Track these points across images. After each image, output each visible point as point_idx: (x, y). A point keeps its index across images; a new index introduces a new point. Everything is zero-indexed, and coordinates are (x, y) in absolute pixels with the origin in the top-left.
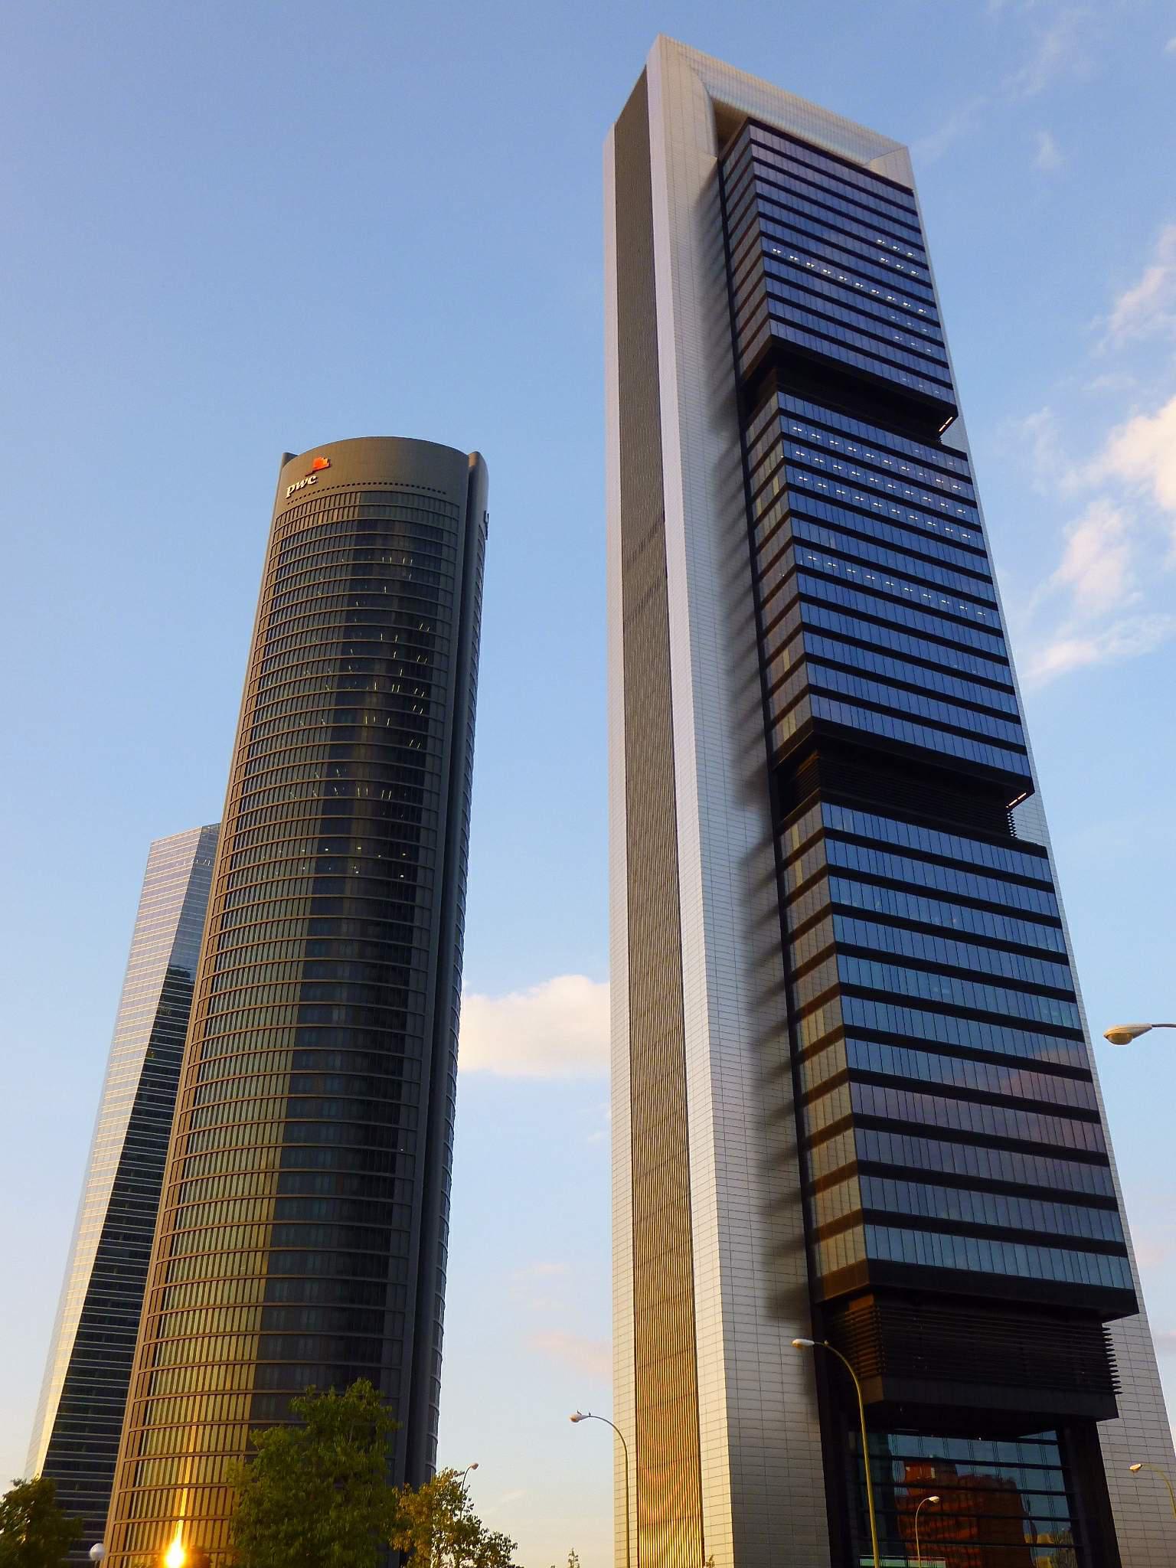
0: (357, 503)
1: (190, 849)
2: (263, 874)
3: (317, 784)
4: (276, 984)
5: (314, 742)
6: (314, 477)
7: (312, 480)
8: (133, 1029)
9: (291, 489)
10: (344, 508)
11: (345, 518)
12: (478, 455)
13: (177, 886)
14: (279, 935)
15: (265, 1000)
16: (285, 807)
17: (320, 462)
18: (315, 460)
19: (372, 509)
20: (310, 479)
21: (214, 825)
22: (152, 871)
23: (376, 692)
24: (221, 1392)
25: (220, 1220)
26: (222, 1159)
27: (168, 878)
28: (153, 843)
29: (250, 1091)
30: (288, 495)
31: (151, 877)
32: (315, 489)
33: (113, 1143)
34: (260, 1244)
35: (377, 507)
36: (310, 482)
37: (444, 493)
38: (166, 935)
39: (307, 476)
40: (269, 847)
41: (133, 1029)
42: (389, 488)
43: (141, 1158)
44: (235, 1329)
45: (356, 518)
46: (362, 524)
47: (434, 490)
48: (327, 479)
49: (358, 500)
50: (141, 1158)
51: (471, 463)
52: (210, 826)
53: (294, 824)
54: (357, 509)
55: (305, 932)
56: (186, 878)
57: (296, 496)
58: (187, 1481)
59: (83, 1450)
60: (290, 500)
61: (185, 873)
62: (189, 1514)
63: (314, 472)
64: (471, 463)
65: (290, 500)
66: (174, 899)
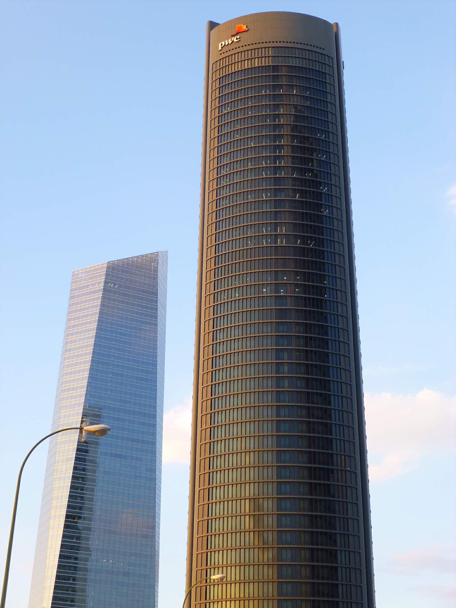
0: (270, 55)
4: (231, 353)
5: (231, 324)
6: (238, 37)
7: (237, 39)
8: (73, 389)
9: (222, 44)
12: (337, 24)
14: (225, 364)
15: (221, 364)
17: (241, 27)
18: (237, 26)
19: (280, 59)
21: (114, 261)
22: (75, 289)
23: (282, 114)
26: (221, 309)
27: (87, 294)
28: (74, 272)
30: (220, 49)
31: (74, 293)
32: (240, 44)
33: (67, 460)
34: (247, 511)
36: (235, 40)
37: (323, 49)
38: (89, 330)
41: (73, 389)
45: (270, 64)
46: (275, 68)
48: (247, 38)
49: (270, 52)
51: (335, 30)
52: (112, 261)
53: (231, 242)
55: (275, 492)
56: (100, 294)
60: (222, 52)
61: (99, 291)
63: (237, 34)
64: (335, 30)
65: (222, 52)
66: (92, 307)
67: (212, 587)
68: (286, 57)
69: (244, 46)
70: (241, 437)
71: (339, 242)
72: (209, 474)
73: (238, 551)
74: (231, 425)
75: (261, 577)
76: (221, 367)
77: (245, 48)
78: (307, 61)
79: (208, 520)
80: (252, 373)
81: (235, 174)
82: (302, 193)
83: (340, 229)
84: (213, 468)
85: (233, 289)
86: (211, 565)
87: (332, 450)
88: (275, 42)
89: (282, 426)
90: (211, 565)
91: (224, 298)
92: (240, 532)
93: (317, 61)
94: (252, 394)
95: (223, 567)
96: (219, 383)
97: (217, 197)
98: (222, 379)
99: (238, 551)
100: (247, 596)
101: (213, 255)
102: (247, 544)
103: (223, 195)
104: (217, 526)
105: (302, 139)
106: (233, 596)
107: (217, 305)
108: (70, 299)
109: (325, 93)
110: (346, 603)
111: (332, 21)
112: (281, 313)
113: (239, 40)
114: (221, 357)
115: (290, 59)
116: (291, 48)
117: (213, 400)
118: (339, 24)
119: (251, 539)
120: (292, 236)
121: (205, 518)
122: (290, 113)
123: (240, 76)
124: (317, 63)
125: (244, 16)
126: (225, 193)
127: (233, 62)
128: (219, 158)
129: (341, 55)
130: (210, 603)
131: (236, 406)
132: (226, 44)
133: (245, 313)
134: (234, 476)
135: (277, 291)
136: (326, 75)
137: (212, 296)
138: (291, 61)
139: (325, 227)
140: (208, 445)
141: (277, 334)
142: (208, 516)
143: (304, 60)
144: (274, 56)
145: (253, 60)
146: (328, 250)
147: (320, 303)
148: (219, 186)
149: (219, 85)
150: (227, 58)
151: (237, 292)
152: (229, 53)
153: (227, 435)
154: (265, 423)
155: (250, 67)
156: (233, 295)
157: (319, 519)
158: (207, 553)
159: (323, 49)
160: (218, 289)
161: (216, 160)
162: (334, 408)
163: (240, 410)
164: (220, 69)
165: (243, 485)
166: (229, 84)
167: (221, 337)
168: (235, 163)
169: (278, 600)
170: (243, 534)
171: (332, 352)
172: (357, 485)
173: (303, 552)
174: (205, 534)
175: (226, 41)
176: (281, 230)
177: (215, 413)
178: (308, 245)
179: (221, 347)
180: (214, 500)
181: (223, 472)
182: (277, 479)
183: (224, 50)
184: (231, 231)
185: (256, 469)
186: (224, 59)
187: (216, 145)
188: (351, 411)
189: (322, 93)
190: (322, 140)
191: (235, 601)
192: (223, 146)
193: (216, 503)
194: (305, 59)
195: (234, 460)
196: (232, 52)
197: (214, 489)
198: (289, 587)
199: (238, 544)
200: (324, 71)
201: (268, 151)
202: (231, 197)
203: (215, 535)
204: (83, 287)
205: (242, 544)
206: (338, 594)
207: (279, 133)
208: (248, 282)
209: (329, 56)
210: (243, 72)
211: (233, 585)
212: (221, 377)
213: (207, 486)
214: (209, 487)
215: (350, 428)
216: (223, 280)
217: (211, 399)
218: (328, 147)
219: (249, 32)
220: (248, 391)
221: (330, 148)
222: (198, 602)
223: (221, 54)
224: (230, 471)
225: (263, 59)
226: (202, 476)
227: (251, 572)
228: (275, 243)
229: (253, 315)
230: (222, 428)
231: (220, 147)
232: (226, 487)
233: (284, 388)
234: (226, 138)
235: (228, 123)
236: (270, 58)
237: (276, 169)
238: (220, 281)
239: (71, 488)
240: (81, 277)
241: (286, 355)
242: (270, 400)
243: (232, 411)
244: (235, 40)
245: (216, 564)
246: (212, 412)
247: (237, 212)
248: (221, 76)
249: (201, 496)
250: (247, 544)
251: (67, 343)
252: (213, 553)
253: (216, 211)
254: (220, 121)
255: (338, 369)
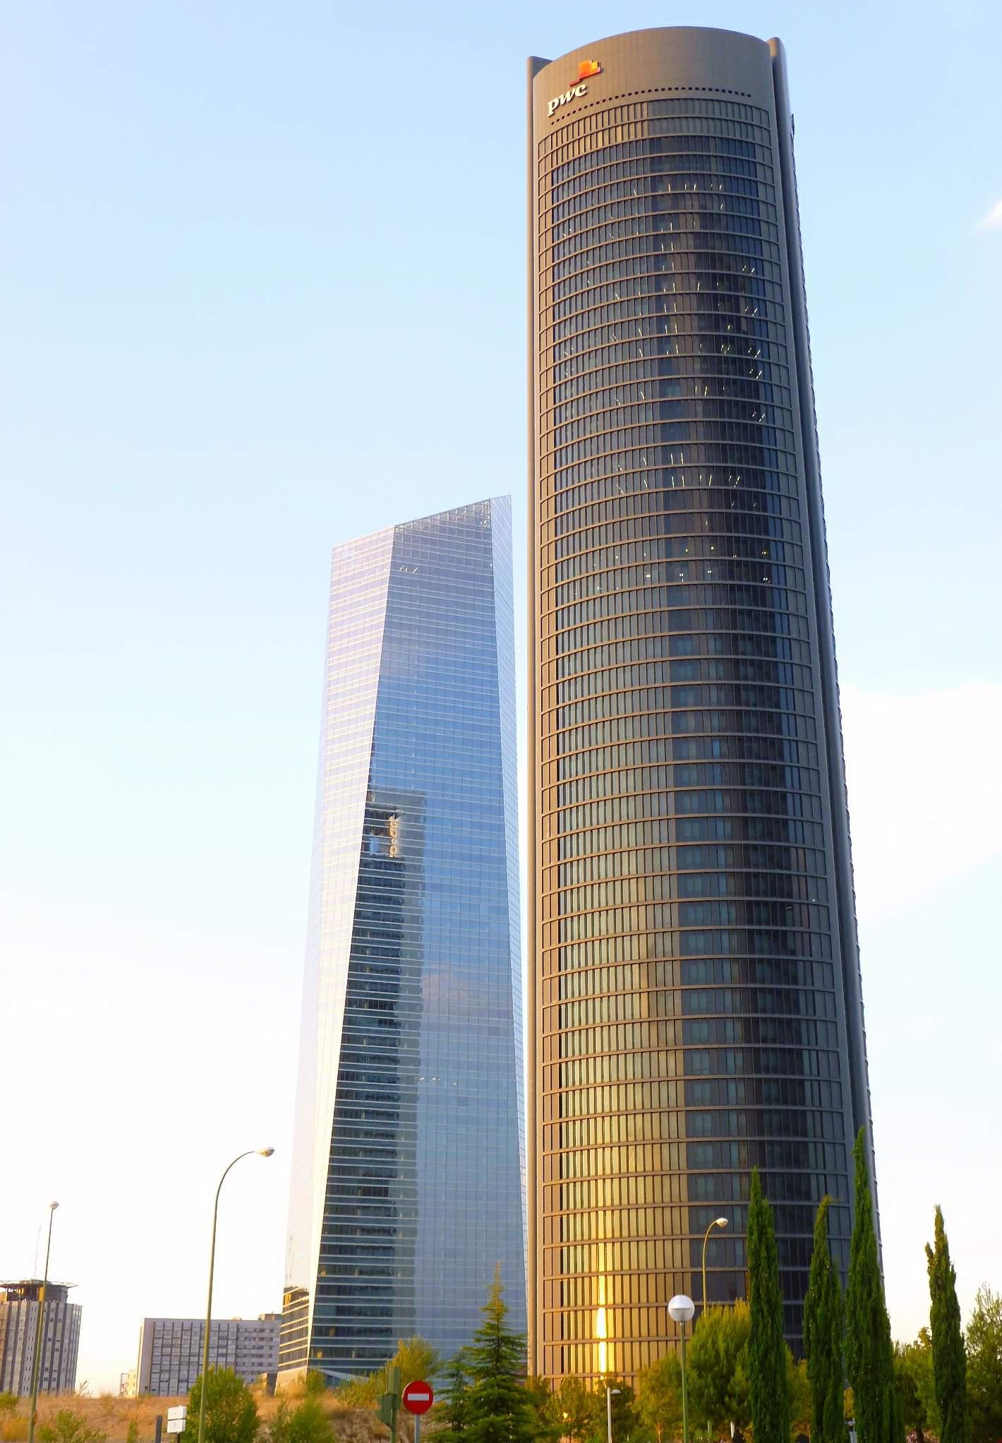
0: (645, 117)
1: (383, 553)
2: (574, 592)
3: (622, 479)
6: (583, 87)
7: (581, 90)
9: (553, 104)
10: (616, 127)
11: (632, 138)
12: (777, 41)
13: (373, 599)
16: (583, 512)
17: (588, 66)
18: (580, 65)
19: (664, 124)
20: (579, 88)
24: (650, 1173)
25: (601, 989)
27: (360, 590)
28: (334, 549)
29: (599, 846)
30: (551, 113)
32: (586, 102)
35: (670, 120)
36: (578, 94)
37: (749, 96)
39: (572, 85)
40: (577, 559)
42: (683, 94)
43: (376, 916)
44: (622, 1107)
45: (646, 136)
46: (655, 143)
47: (724, 91)
48: (601, 88)
49: (645, 112)
50: (376, 916)
51: (772, 53)
52: (404, 524)
54: (645, 124)
57: (559, 114)
58: (602, 1269)
59: (358, 1233)
62: (611, 1301)
63: (581, 80)
64: (772, 53)
67: (571, 1124)
68: (676, 120)
69: (595, 104)
70: (615, 938)
71: (769, 242)
72: (559, 867)
73: (614, 1058)
74: (596, 887)
75: (655, 1104)
76: (573, 726)
77: (598, 108)
78: (718, 123)
79: (560, 977)
80: (630, 734)
81: (586, 357)
82: (717, 385)
83: (776, 280)
84: (566, 1027)
85: (591, 701)
86: (566, 1056)
87: (788, 840)
88: (653, 90)
89: (688, 828)
90: (566, 1056)
91: (574, 597)
92: (615, 909)
93: (737, 122)
94: (631, 799)
95: (588, 1089)
96: (570, 782)
97: (555, 425)
98: (576, 723)
99: (614, 1058)
100: (631, 1107)
101: (552, 427)
102: (629, 1046)
103: (566, 399)
104: (575, 1014)
105: (713, 259)
106: (607, 1140)
107: (563, 609)
108: (332, 586)
109: (752, 165)
110: (821, 1145)
111: (765, 37)
112: (678, 618)
113: (584, 93)
114: (574, 758)
115: (684, 122)
116: (686, 99)
117: (562, 867)
118: (783, 41)
119: (638, 1036)
120: (719, 765)
121: (555, 1002)
122: (691, 354)
123: (588, 164)
124: (737, 126)
125: (594, 44)
126: (570, 394)
127: (576, 137)
128: (557, 369)
129: (786, 99)
130: (568, 1215)
131: (602, 797)
132: (562, 103)
133: (611, 574)
134: (601, 815)
135: (666, 483)
136: (758, 168)
137: (553, 593)
138: (684, 128)
139: (771, 517)
140: (555, 870)
141: (675, 658)
142: (560, 999)
143: (711, 122)
144: (653, 120)
145: (613, 131)
146: (774, 515)
147: (759, 595)
148: (558, 321)
149: (553, 242)
150: (565, 130)
151: (597, 583)
152: (568, 121)
153: (588, 850)
154: (654, 770)
155: (607, 144)
156: (591, 589)
157: (748, 796)
158: (560, 1064)
159: (749, 96)
160: (562, 580)
161: (550, 292)
162: (792, 791)
163: (609, 803)
164: (552, 153)
165: (619, 940)
166: (569, 182)
167: (571, 669)
168: (586, 336)
169: (688, 1174)
170: (621, 1028)
171: (789, 738)
172: (814, 713)
173: (720, 825)
174: (556, 1031)
175: (562, 97)
176: (677, 460)
177: (565, 891)
178: (726, 483)
179: (572, 663)
180: (569, 970)
181: (582, 918)
182: (682, 984)
183: (558, 115)
184: (581, 401)
185: (640, 826)
186: (560, 133)
187: (550, 303)
188: (806, 640)
189: (746, 165)
190: (750, 278)
191: (611, 1117)
192: (564, 495)
193: (572, 974)
194: (713, 119)
195: (601, 788)
196: (574, 118)
197: (569, 949)
198: (711, 1181)
199: (614, 1047)
200: (750, 140)
201: (646, 308)
202: (581, 401)
203: (573, 1002)
204: (353, 578)
205: (621, 1046)
206: (803, 1097)
207: (672, 355)
208: (618, 563)
209: (760, 109)
210: (594, 156)
211: (608, 1182)
212: (575, 743)
213: (555, 945)
214: (560, 974)
215: (793, 523)
216: (571, 562)
217: (558, 786)
218: (755, 212)
219: (603, 75)
220: (621, 689)
221: (765, 272)
222: (548, 1151)
223: (553, 123)
224: (596, 915)
225: (632, 127)
226: (547, 927)
227: (636, 1097)
228: (665, 486)
229: (625, 577)
230: (580, 1005)
231: (559, 474)
232: (590, 944)
233: (688, 759)
234: (567, 290)
235: (570, 259)
236: (645, 124)
237: (663, 342)
238: (565, 564)
239: (331, 1153)
240: (348, 558)
241: (691, 697)
242: (663, 782)
243: (594, 805)
244: (578, 94)
245: (577, 1083)
246: (560, 836)
247: (593, 429)
248: (555, 166)
249: (547, 991)
250: (629, 1046)
251: (329, 684)
252: (570, 1064)
253: (556, 518)
254: (555, 199)
255: (785, 640)
